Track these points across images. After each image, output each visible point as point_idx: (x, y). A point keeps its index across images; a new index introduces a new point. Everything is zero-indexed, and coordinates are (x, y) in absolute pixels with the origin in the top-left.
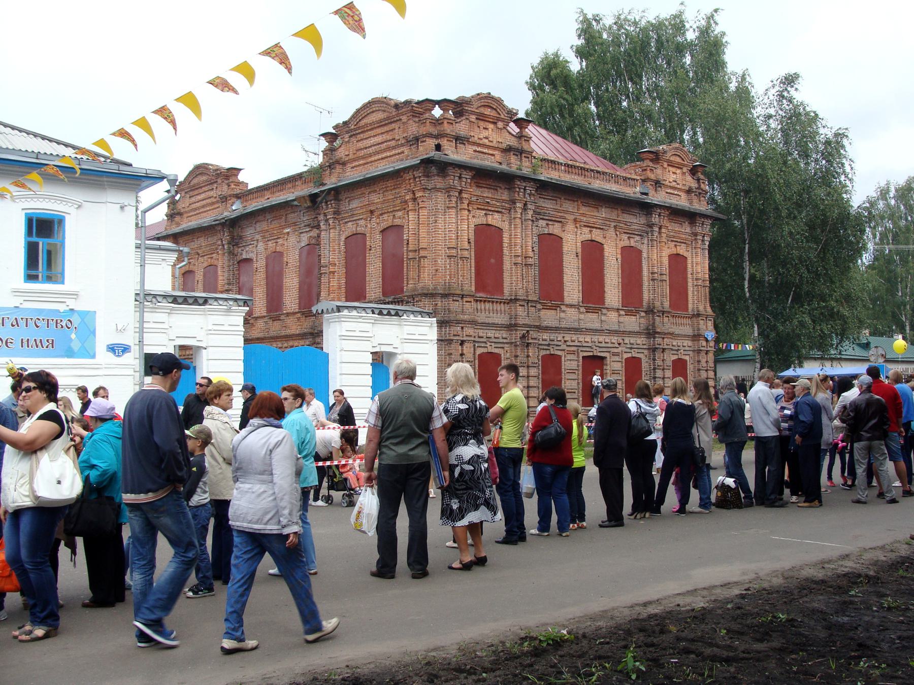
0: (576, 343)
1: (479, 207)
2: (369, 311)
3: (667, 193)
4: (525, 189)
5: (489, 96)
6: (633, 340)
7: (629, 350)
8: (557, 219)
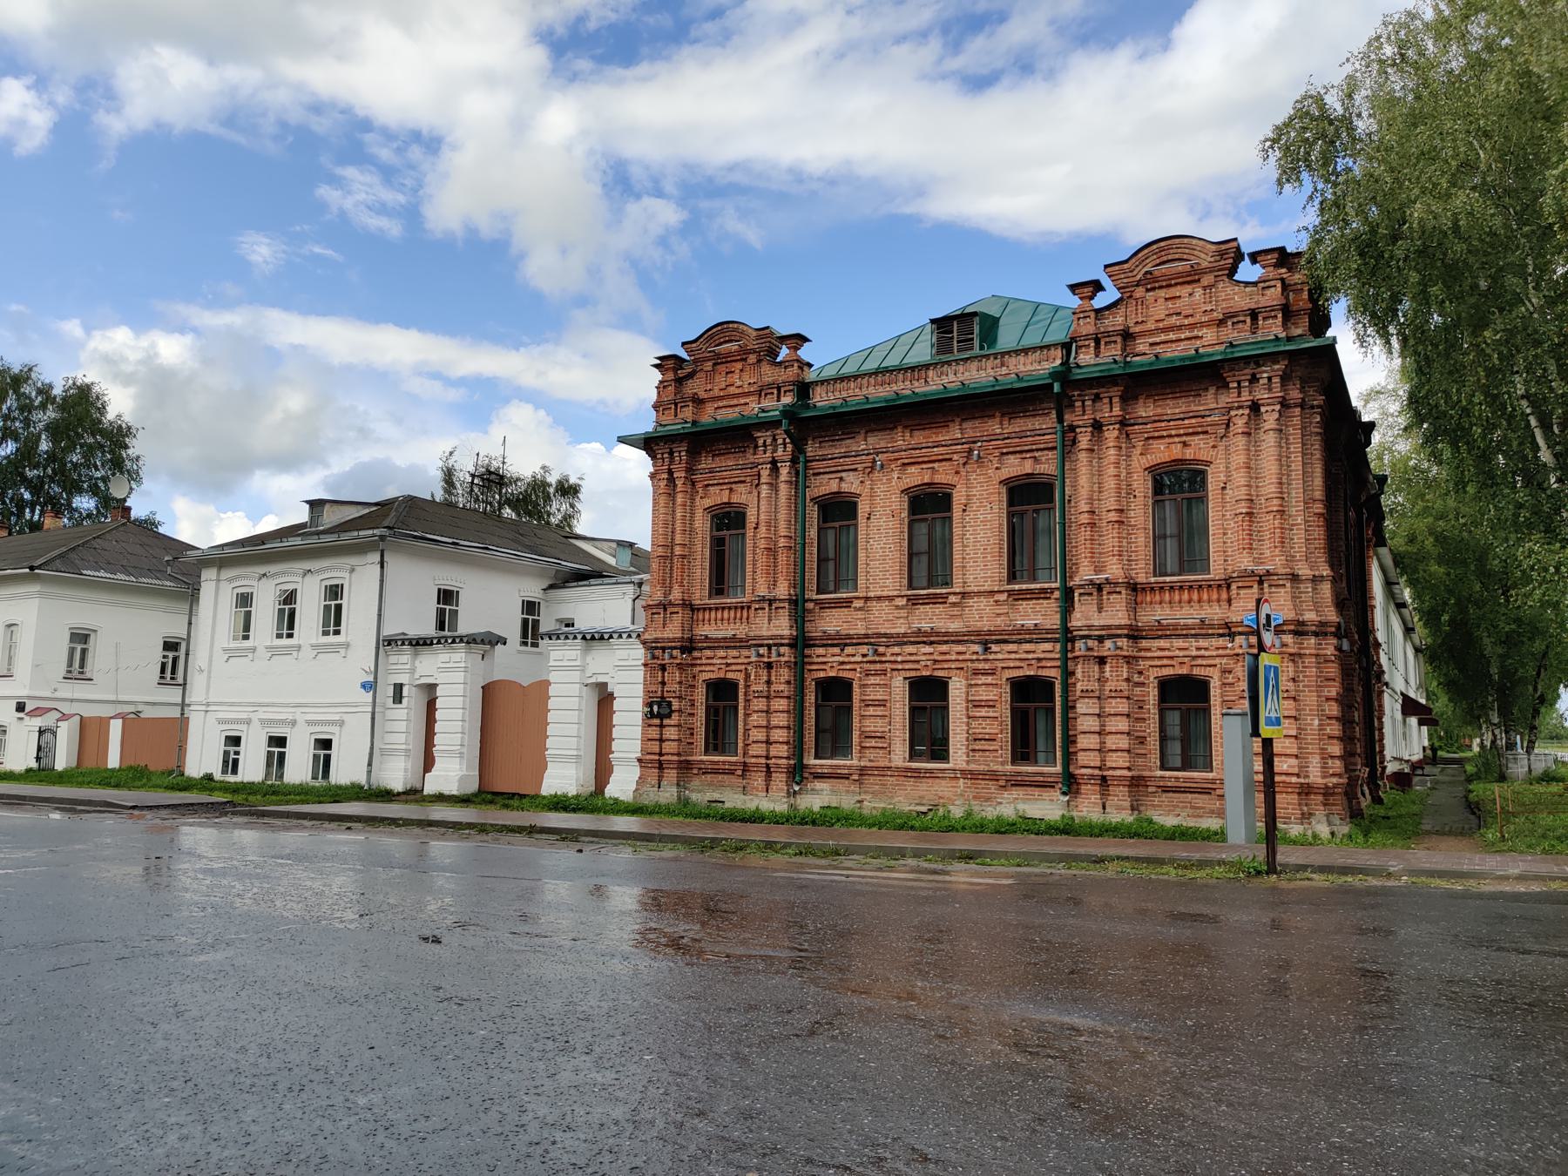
4: (775, 440)
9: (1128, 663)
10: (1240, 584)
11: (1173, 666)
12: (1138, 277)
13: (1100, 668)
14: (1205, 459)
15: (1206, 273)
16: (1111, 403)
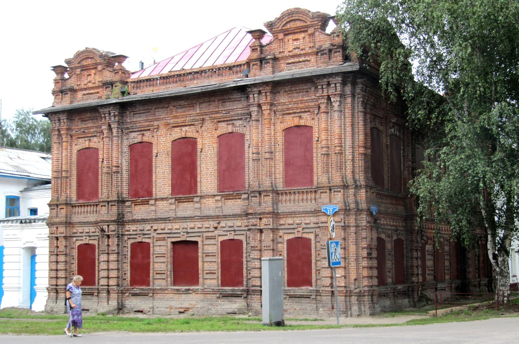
0: (166, 231)
1: (219, 120)
2: (15, 221)
4: (110, 114)
6: (230, 223)
7: (225, 233)
8: (145, 129)
9: (273, 232)
10: (321, 191)
11: (294, 233)
12: (280, 28)
14: (309, 125)
15: (310, 27)
16: (266, 96)
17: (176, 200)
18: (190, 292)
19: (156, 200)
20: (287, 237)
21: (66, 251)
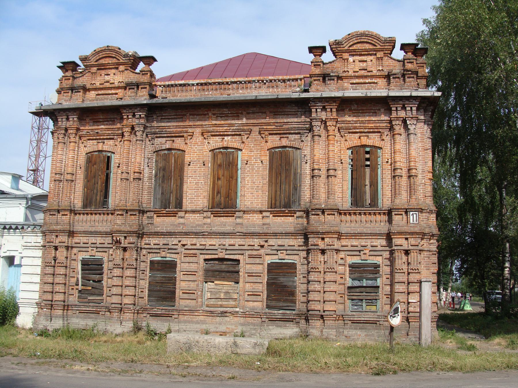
3: (352, 84)
5: (108, 49)
6: (280, 242)
7: (275, 252)
10: (396, 213)
12: (346, 48)
13: (55, 252)
15: (379, 51)
17: (212, 214)
18: (228, 314)
19: (186, 212)
20: (81, 256)
21: (67, 263)
